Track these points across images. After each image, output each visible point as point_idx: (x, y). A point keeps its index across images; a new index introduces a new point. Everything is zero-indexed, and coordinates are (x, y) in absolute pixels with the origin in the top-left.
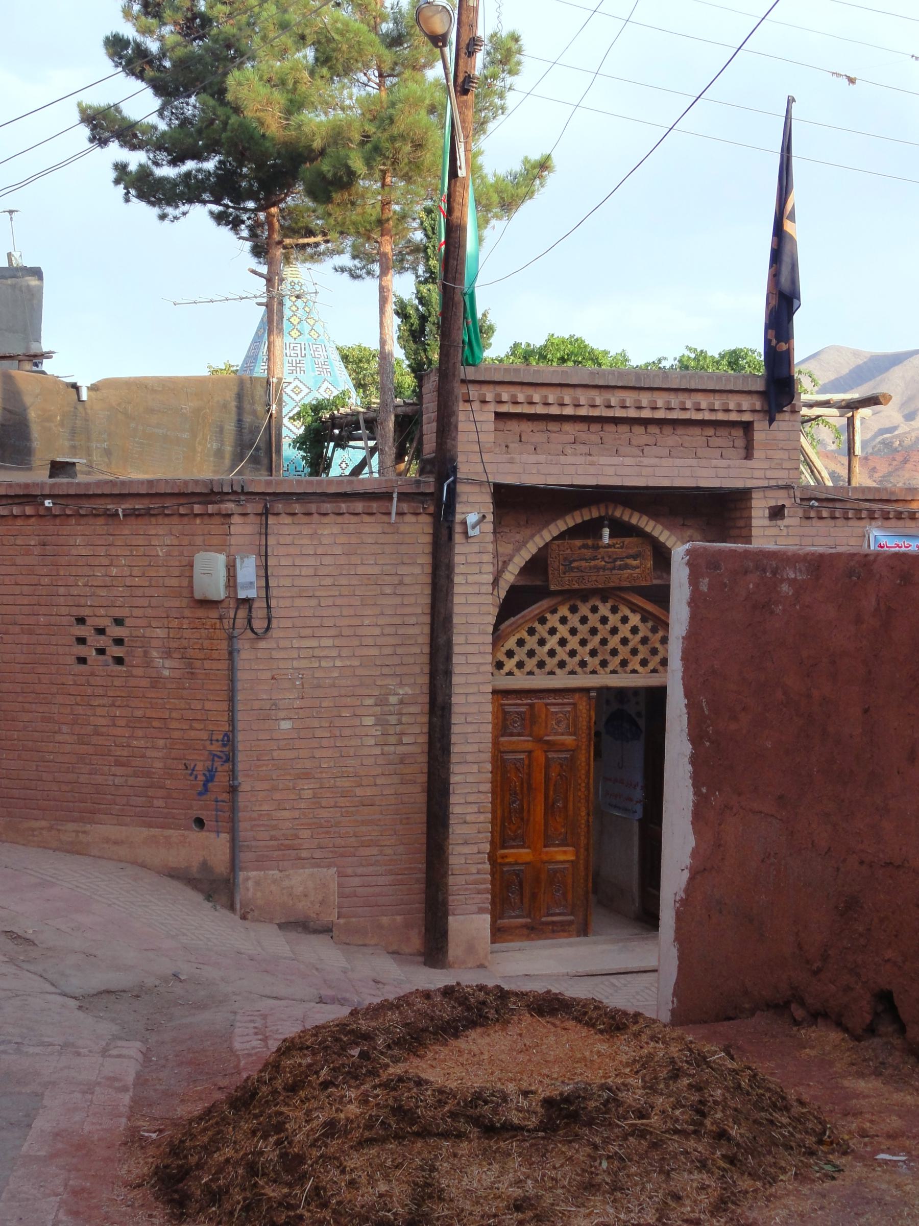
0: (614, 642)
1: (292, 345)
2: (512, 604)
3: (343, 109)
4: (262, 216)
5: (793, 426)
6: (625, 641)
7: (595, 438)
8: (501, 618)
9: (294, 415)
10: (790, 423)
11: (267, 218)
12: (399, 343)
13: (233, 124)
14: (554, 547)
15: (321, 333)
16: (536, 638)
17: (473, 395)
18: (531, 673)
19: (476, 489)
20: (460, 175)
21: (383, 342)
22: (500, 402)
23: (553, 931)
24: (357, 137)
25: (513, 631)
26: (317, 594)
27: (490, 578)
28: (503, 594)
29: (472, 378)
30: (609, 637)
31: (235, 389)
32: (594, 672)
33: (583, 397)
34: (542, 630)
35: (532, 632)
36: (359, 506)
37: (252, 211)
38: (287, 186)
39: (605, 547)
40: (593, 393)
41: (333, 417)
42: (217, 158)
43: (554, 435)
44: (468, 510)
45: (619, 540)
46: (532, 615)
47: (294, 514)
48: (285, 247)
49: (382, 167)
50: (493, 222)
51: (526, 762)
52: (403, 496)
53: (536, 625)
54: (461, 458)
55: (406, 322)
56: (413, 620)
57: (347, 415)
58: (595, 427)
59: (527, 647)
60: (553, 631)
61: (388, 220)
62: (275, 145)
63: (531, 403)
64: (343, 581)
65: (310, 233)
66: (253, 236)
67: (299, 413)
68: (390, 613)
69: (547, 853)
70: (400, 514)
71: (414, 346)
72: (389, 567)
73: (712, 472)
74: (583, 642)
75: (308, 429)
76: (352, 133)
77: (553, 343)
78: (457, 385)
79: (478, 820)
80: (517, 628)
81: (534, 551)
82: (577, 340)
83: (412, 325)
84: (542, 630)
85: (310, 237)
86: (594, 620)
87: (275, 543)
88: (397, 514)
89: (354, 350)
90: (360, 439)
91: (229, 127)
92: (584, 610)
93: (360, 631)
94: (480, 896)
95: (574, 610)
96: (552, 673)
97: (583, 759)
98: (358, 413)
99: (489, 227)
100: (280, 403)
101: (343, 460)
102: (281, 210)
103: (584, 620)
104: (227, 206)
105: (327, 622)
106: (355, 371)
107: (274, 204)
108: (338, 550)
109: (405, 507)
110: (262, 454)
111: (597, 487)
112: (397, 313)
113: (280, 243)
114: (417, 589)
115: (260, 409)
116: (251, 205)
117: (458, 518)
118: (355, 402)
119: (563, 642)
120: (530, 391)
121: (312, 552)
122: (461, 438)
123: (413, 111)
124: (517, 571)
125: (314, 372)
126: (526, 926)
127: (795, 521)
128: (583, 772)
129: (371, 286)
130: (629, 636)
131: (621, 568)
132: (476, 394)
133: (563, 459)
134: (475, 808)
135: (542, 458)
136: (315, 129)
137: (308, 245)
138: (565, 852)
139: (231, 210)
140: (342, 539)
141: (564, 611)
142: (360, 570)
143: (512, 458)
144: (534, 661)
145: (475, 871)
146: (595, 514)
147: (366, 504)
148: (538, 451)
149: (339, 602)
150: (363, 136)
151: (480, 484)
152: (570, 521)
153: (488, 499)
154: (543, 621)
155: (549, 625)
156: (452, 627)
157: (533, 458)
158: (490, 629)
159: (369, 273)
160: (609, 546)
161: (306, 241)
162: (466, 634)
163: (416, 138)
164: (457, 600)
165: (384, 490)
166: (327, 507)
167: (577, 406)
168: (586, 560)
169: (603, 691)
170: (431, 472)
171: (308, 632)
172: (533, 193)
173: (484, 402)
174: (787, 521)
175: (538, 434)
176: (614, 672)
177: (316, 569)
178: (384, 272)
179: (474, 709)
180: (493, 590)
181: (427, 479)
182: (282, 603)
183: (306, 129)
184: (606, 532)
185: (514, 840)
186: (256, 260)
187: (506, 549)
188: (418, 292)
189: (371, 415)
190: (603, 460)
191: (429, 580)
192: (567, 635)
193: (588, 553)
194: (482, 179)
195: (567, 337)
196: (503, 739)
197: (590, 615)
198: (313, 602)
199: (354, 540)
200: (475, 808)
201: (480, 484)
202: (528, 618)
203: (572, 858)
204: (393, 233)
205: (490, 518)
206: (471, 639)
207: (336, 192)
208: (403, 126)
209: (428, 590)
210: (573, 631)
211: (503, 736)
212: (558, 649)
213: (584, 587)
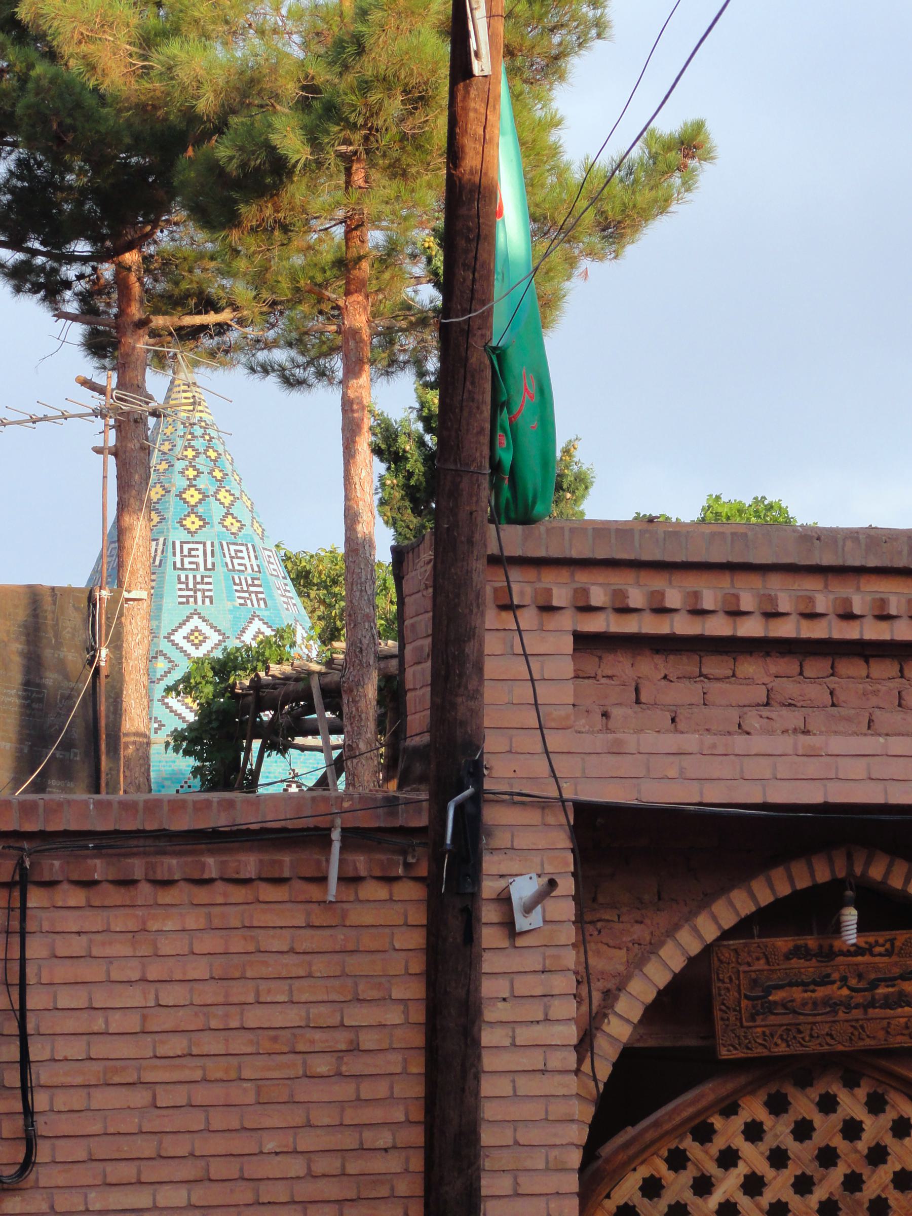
1: (186, 547)
2: (630, 1095)
3: (261, 33)
4: (107, 271)
7: (817, 692)
8: (601, 1130)
9: (178, 683)
11: (117, 275)
12: (382, 514)
13: (39, 78)
14: (726, 954)
15: (247, 521)
16: (686, 1178)
17: (522, 593)
19: (532, 817)
20: (476, 71)
21: (351, 518)
22: (587, 609)
24: (291, 89)
25: (631, 1159)
26: (149, 1077)
27: (571, 1034)
28: (604, 1071)
29: (518, 552)
30: (865, 1171)
31: (22, 615)
33: (785, 593)
34: (703, 1157)
35: (677, 1160)
36: (249, 863)
37: (84, 260)
38: (155, 211)
39: (849, 953)
40: (809, 584)
41: (256, 684)
42: (14, 156)
43: (717, 685)
44: (515, 867)
45: (881, 937)
46: (677, 1120)
47: (90, 884)
48: (154, 334)
49: (343, 148)
50: (585, 263)
52: (355, 837)
53: (689, 1144)
54: (492, 743)
55: (397, 470)
56: (384, 1139)
57: (287, 678)
58: (815, 667)
60: (728, 1158)
61: (360, 258)
62: (120, 111)
63: (662, 611)
64: (212, 1044)
65: (208, 304)
66: (89, 311)
67: (186, 679)
68: (326, 1121)
70: (349, 880)
71: (414, 521)
72: (322, 1009)
75: (207, 712)
76: (281, 82)
77: (718, 514)
78: (479, 565)
80: (640, 1152)
81: (677, 964)
82: (770, 507)
83: (410, 475)
84: (703, 1157)
85: (207, 312)
86: (826, 1129)
87: (44, 953)
88: (340, 879)
89: (321, 560)
90: (315, 732)
91: (30, 85)
92: (803, 1105)
93: (254, 1169)
95: (778, 1105)
98: (310, 673)
99: (576, 273)
100: (117, 645)
101: (289, 771)
102: (147, 259)
103: (803, 1130)
104: (34, 253)
105: (173, 1147)
106: (322, 602)
107: (129, 247)
108: (198, 969)
109: (361, 863)
110: (77, 755)
111: (826, 807)
112: (377, 451)
113: (142, 324)
114: (393, 1062)
115: (73, 657)
116: (82, 247)
117: (489, 887)
118: (307, 651)
120: (657, 582)
121: (135, 976)
122: (491, 694)
123: (405, 26)
124: (636, 1015)
125: (230, 598)
129: (325, 400)
131: (888, 1003)
132: (528, 589)
133: (740, 743)
135: (690, 741)
136: (201, 72)
137: (203, 328)
139: (40, 260)
140: (209, 943)
141: (754, 1109)
142: (255, 1017)
146: (823, 875)
147: (267, 857)
148: (681, 725)
149: (201, 1095)
150: (304, 88)
151: (542, 804)
152: (763, 892)
153: (563, 840)
154: (704, 1134)
155: (718, 1144)
156: (477, 1156)
157: (670, 741)
158: (575, 1158)
159: (321, 374)
160: (858, 950)
161: (198, 320)
162: (515, 1172)
163: (413, 82)
164: (488, 1087)
165: (310, 823)
166: (172, 865)
167: (772, 615)
168: (804, 984)
170: (422, 779)
171: (127, 1172)
172: (667, 200)
173: (547, 609)
175: (680, 685)
177: (144, 1018)
178: (353, 369)
180: (580, 1061)
181: (413, 796)
182: (62, 1101)
183: (183, 74)
184: (850, 916)
186: (94, 362)
187: (608, 961)
188: (423, 405)
189: (335, 676)
190: (837, 744)
191: (419, 1039)
192: (763, 1168)
193: (807, 968)
194: (560, 176)
195: (748, 501)
197: (817, 1119)
198: (140, 1098)
199: (237, 945)
201: (542, 804)
202: (667, 1127)
204: (373, 286)
205: (567, 885)
206: (528, 1184)
207: (247, 202)
208: (384, 58)
209: (418, 1067)
210: (778, 1158)
212: (712, 1168)
213: (799, 1050)
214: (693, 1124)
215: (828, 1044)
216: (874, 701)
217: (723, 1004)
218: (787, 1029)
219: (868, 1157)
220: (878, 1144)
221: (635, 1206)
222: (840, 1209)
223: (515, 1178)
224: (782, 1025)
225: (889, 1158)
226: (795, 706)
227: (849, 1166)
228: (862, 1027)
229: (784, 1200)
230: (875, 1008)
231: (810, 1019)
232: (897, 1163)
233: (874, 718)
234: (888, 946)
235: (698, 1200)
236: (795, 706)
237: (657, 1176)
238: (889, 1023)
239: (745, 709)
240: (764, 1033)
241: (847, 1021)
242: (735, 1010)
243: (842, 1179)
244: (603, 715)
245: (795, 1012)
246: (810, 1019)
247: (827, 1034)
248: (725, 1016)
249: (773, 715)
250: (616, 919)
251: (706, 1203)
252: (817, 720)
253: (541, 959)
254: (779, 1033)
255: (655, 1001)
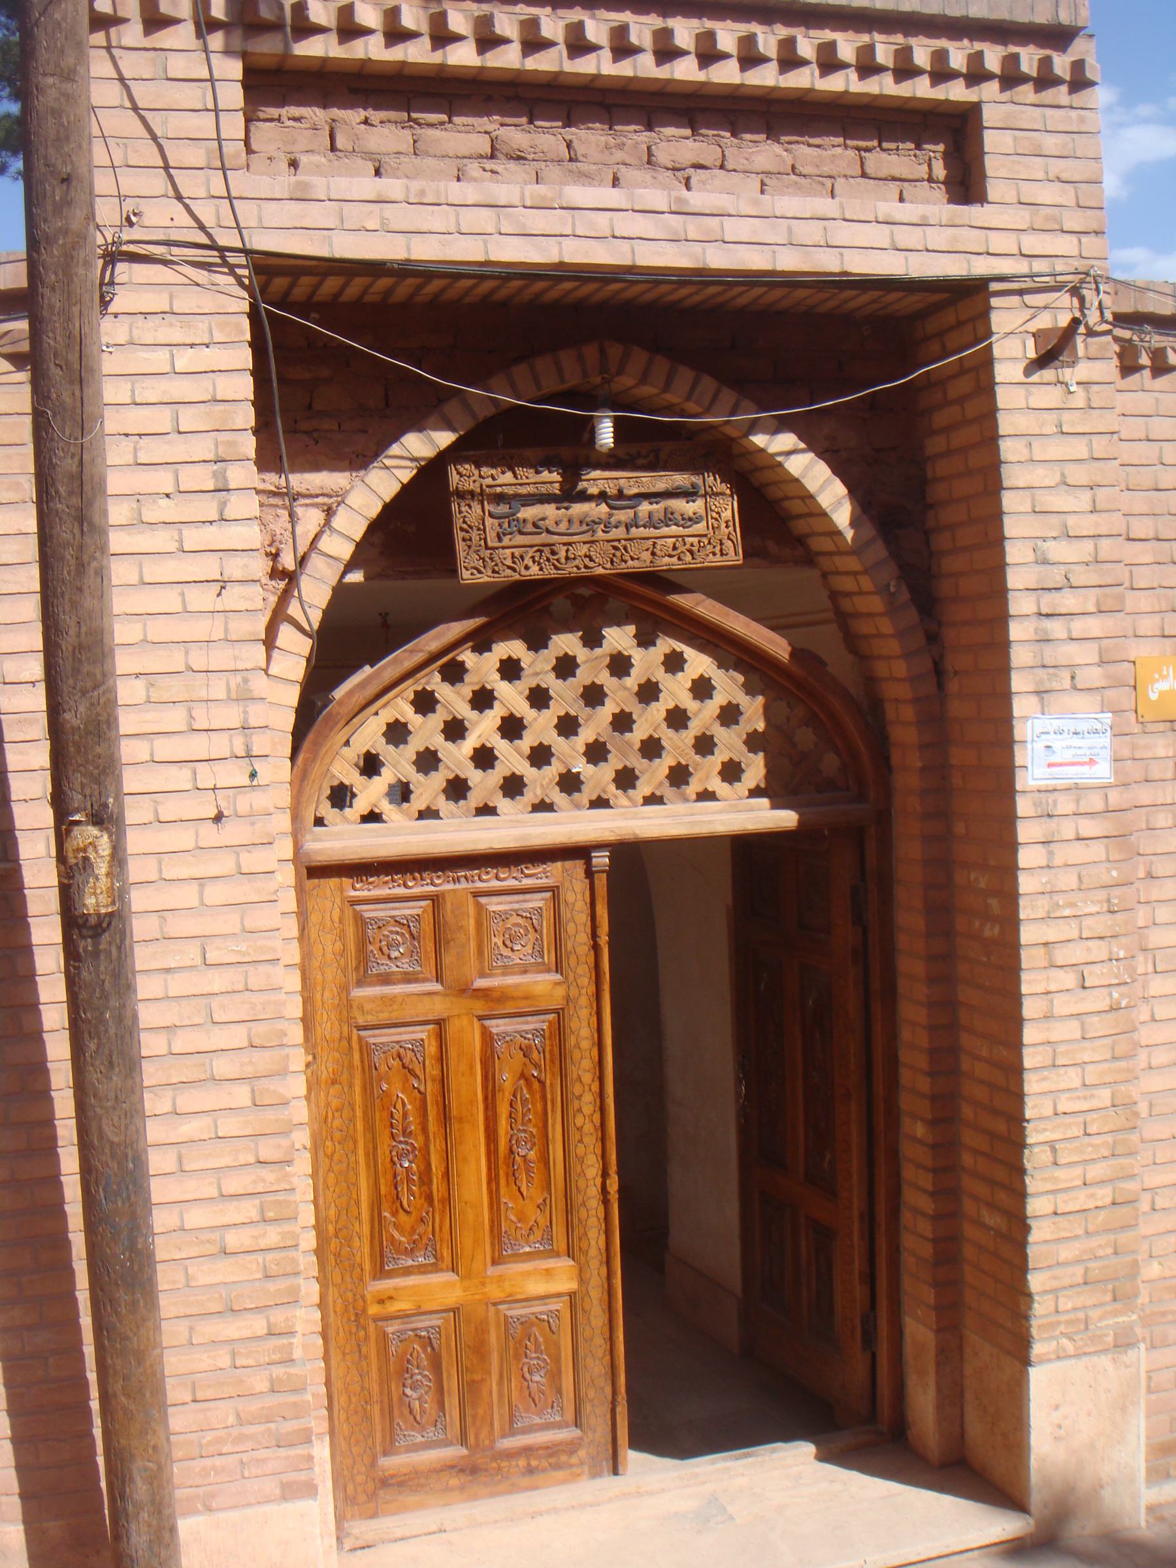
0: (649, 721)
5: (1082, 120)
6: (677, 719)
10: (1074, 114)
16: (436, 720)
18: (428, 814)
23: (530, 1471)
32: (600, 803)
34: (454, 700)
35: (425, 703)
51: (432, 1048)
59: (415, 745)
69: (501, 1279)
73: (878, 235)
74: (568, 726)
79: (263, 1244)
94: (282, 1452)
96: (486, 810)
97: (585, 1032)
119: (512, 728)
126: (451, 1467)
127: (1108, 369)
128: (587, 1064)
130: (689, 703)
134: (249, 1210)
135: (392, 186)
138: (548, 1273)
143: (304, 186)
144: (438, 779)
145: (264, 1386)
154: (454, 673)
169: (629, 854)
174: (1083, 370)
175: (380, 129)
176: (653, 800)
179: (229, 923)
185: (410, 1253)
190: (578, 194)
192: (522, 708)
196: (358, 993)
200: (249, 1210)
203: (573, 1286)
210: (539, 698)
211: (360, 983)
212: (502, 746)
214: (440, 663)
215: (586, 567)
216: (619, 155)
217: (464, 522)
218: (538, 551)
219: (638, 694)
220: (649, 680)
221: (378, 754)
222: (609, 752)
223: (189, 711)
224: (532, 546)
225: (661, 695)
226: (525, 159)
227: (618, 705)
228: (625, 548)
229: (546, 743)
230: (637, 527)
231: (565, 539)
232: (670, 700)
233: (619, 175)
234: (651, 457)
235: (449, 745)
236: (525, 159)
237: (403, 720)
238: (655, 543)
239: (465, 160)
240: (513, 554)
241: (608, 541)
242: (479, 529)
243: (667, 772)
244: (290, 165)
245: (548, 531)
246: (565, 539)
247: (586, 556)
248: (467, 536)
249: (499, 168)
250: (336, 427)
251: (460, 749)
252: (552, 172)
253: (212, 447)
254: (530, 555)
255: (381, 515)
